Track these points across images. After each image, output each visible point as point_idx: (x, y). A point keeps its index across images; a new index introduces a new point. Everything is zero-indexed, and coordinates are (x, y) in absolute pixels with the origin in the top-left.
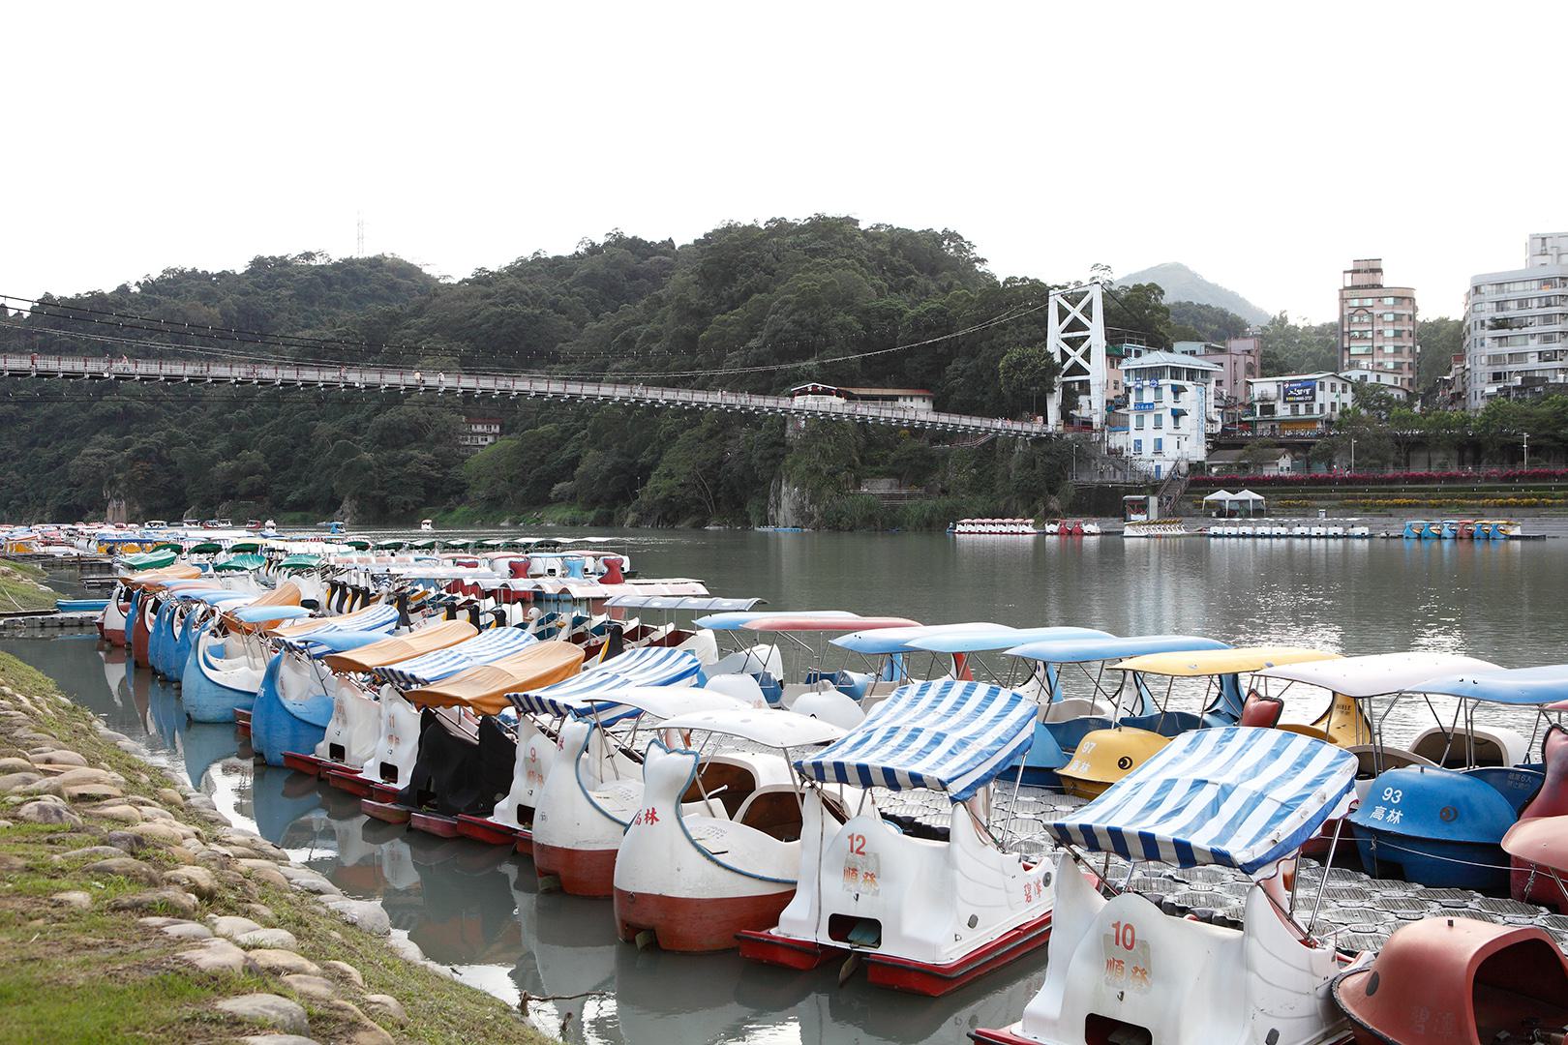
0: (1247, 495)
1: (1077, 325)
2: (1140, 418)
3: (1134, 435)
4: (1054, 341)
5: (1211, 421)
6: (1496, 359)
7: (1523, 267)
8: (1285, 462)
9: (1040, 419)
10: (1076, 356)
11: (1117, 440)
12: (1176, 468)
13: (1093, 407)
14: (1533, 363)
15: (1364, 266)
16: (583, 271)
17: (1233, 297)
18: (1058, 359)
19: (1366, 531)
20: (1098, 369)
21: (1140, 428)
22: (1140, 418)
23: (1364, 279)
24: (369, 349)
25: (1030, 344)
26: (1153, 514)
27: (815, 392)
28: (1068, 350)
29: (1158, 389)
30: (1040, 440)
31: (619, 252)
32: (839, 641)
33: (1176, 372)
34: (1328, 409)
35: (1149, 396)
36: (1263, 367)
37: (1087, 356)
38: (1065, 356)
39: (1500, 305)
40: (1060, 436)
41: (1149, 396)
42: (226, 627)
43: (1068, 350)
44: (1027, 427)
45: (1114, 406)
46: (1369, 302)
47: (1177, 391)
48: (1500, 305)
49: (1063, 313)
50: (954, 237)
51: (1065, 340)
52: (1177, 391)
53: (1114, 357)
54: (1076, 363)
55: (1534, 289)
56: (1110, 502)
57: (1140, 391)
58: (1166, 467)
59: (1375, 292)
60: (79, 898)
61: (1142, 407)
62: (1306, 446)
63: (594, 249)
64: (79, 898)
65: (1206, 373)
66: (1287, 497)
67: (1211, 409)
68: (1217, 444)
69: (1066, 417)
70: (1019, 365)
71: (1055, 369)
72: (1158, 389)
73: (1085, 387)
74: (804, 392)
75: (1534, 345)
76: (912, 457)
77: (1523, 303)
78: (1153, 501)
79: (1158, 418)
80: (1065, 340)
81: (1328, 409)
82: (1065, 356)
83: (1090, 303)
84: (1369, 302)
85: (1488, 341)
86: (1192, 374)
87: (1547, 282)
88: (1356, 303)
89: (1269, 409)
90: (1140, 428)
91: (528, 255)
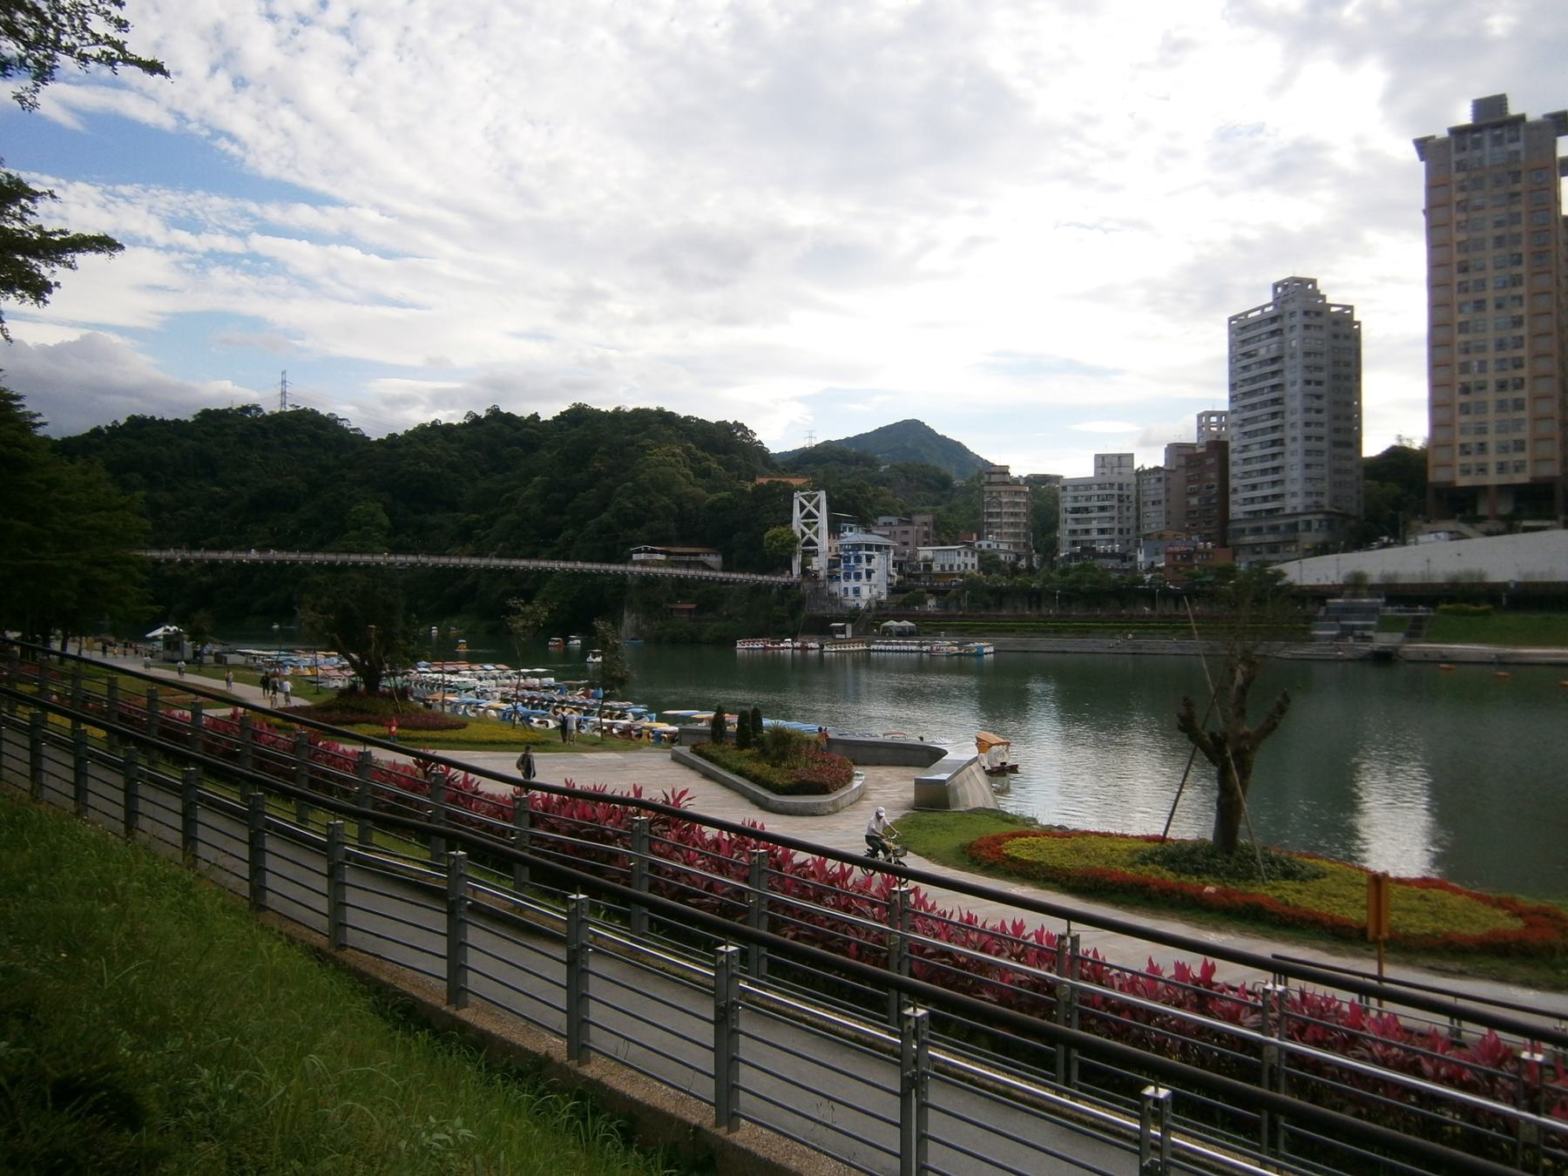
0: (905, 623)
1: (810, 515)
6: (1074, 532)
7: (1092, 474)
8: (931, 603)
11: (835, 588)
12: (869, 602)
13: (819, 564)
19: (1098, 562)
20: (824, 542)
24: (973, 1030)
25: (783, 525)
26: (849, 635)
27: (646, 551)
30: (787, 587)
31: (496, 425)
33: (869, 547)
37: (816, 533)
38: (803, 534)
39: (1076, 499)
40: (799, 585)
44: (779, 579)
45: (833, 564)
47: (869, 559)
48: (1076, 499)
49: (802, 507)
50: (741, 427)
53: (835, 529)
55: (1095, 491)
56: (822, 628)
58: (863, 605)
62: (945, 593)
63: (476, 421)
65: (887, 547)
66: (927, 627)
68: (893, 590)
70: (774, 538)
71: (796, 541)
74: (639, 552)
75: (1094, 525)
76: (709, 598)
77: (1088, 499)
78: (849, 626)
82: (803, 534)
86: (879, 548)
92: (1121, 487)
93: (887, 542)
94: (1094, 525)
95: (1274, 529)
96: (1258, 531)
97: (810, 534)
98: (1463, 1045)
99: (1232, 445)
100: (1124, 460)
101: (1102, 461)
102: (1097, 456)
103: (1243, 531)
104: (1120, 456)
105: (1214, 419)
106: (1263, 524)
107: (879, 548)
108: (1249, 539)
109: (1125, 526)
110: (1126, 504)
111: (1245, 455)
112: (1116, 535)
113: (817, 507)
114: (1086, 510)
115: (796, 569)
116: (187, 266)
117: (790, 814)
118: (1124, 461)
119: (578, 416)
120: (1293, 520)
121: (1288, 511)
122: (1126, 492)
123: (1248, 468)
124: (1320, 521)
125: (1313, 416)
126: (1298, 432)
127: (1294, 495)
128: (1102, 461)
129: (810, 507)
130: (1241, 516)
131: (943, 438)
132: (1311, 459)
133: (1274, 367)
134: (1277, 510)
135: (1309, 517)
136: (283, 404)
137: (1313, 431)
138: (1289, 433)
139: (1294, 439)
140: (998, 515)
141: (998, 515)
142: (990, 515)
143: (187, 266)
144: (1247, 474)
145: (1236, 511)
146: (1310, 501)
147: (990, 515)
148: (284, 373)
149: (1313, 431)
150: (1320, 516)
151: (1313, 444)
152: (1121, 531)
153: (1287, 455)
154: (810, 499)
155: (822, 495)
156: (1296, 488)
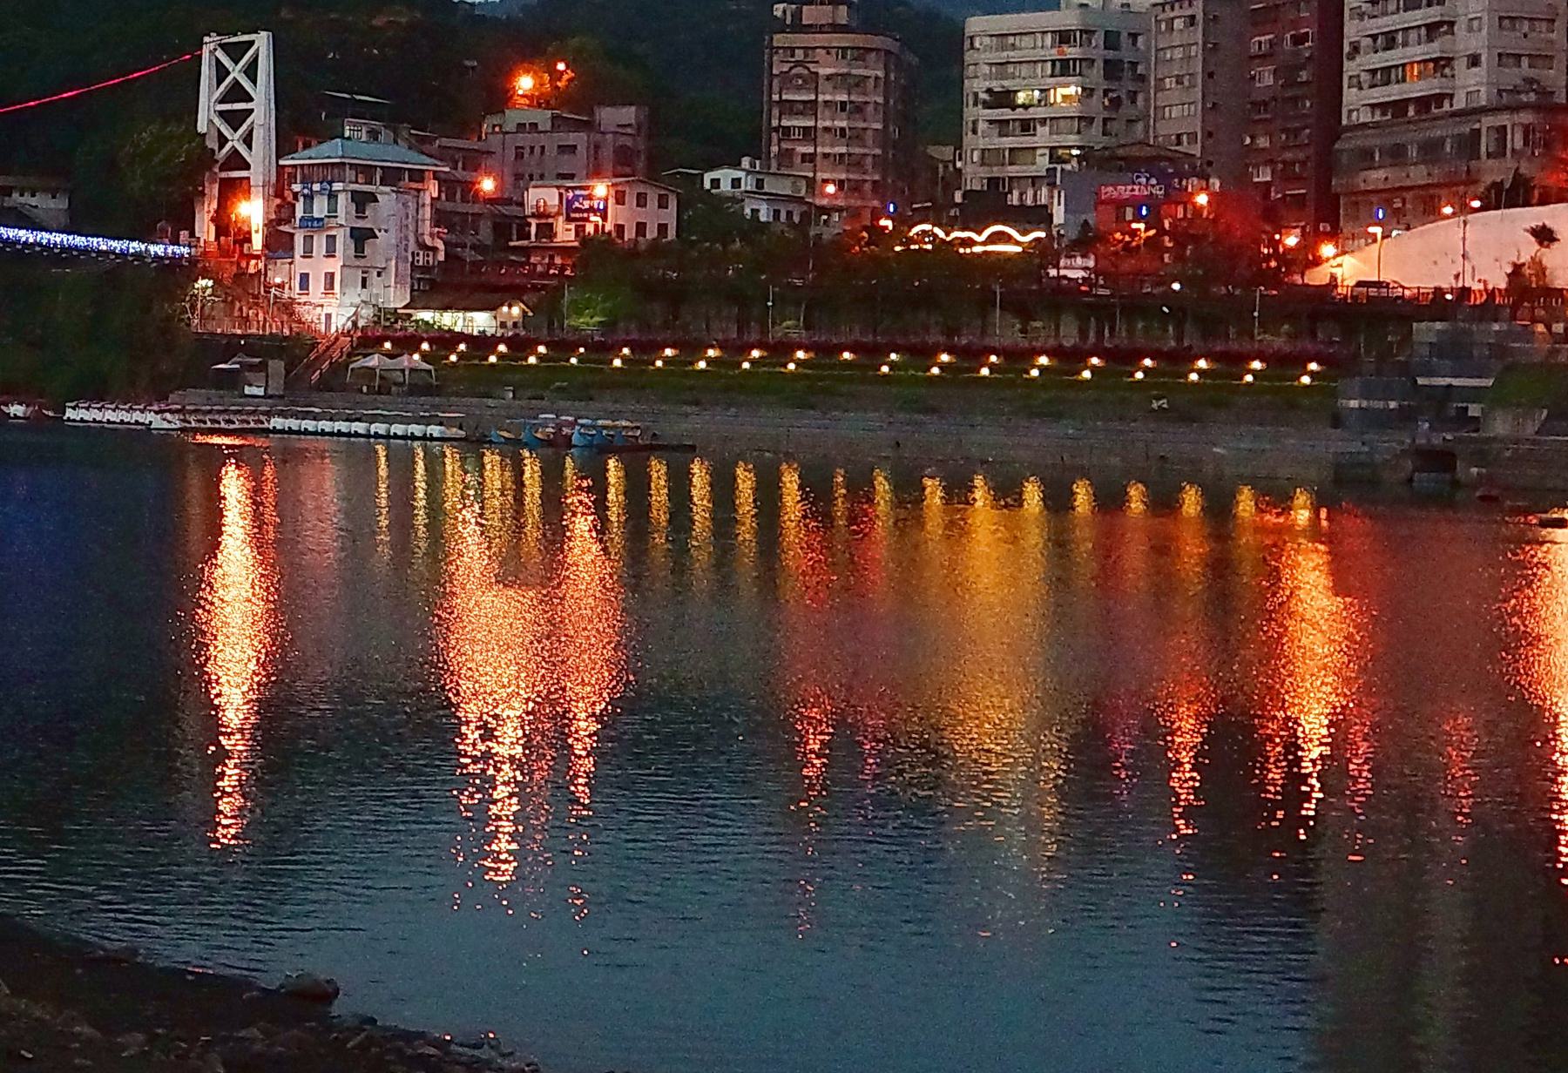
2: (308, 240)
3: (301, 265)
4: (207, 114)
5: (423, 246)
18: (212, 143)
21: (308, 254)
22: (308, 240)
29: (332, 196)
33: (367, 172)
35: (320, 208)
36: (651, 159)
37: (248, 140)
41: (320, 208)
49: (222, 72)
51: (221, 114)
52: (362, 201)
57: (309, 198)
60: (846, 355)
61: (311, 223)
64: (846, 355)
65: (417, 176)
67: (427, 227)
72: (332, 196)
79: (331, 239)
80: (221, 114)
82: (223, 140)
83: (255, 60)
85: (982, 126)
89: (547, 230)
90: (308, 254)
93: (417, 161)
96: (1396, 155)
97: (235, 140)
107: (391, 177)
108: (1376, 177)
113: (251, 72)
115: (205, 230)
116: (468, 761)
121: (1460, 103)
124: (1527, 130)
130: (1365, 117)
134: (1439, 99)
135: (1504, 119)
140: (810, 108)
141: (810, 108)
142: (789, 108)
143: (468, 761)
145: (1357, 102)
146: (1513, 76)
147: (789, 108)
150: (1526, 117)
155: (262, 42)
156: (1477, 42)
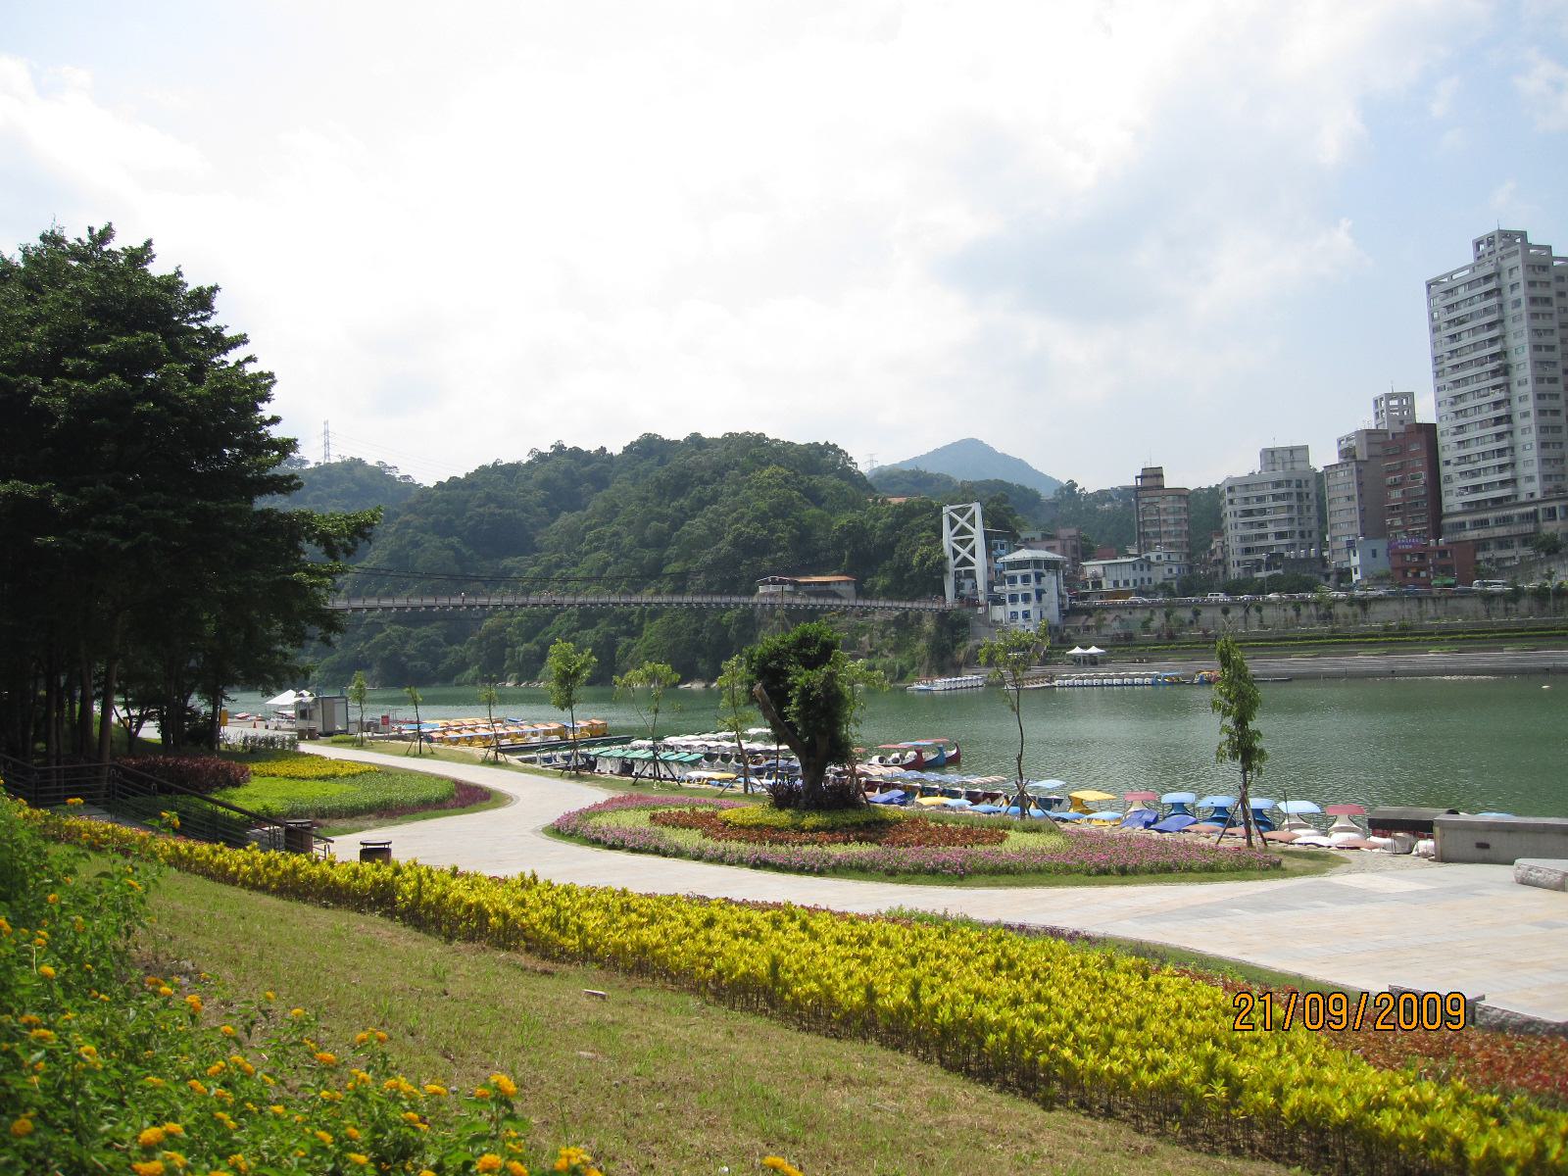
1: (963, 531)
6: (1244, 539)
9: (941, 597)
10: (964, 552)
14: (1272, 541)
15: (1150, 473)
16: (538, 476)
17: (1020, 465)
20: (980, 563)
23: (1149, 482)
27: (774, 582)
28: (958, 548)
32: (262, 503)
34: (1139, 583)
37: (972, 553)
42: (255, 774)
43: (958, 548)
46: (1156, 499)
47: (1039, 577)
49: (953, 523)
54: (965, 558)
59: (1160, 492)
63: (542, 457)
69: (959, 596)
73: (971, 574)
75: (1271, 529)
80: (955, 541)
81: (1139, 583)
82: (956, 553)
84: (1156, 499)
85: (1240, 526)
87: (1278, 484)
88: (1147, 500)
91: (489, 462)
92: (1299, 486)
94: (1271, 529)
95: (1506, 521)
96: (1482, 524)
98: (204, 1121)
99: (1440, 428)
100: (1298, 453)
101: (1270, 456)
102: (1306, 448)
103: (1462, 525)
104: (1292, 450)
105: (1394, 403)
106: (1490, 515)
109: (1306, 528)
110: (1306, 503)
111: (1460, 438)
112: (1297, 538)
114: (1263, 512)
117: (821, 873)
118: (1297, 455)
119: (649, 448)
120: (1531, 509)
121: (1523, 498)
122: (1305, 490)
123: (1464, 452)
125: (1546, 387)
126: (1529, 405)
127: (1530, 479)
128: (1270, 456)
129: (962, 521)
130: (1458, 508)
131: (1004, 456)
132: (1549, 437)
133: (1494, 333)
134: (1507, 498)
136: (327, 455)
137: (1548, 403)
138: (1519, 407)
139: (1526, 415)
144: (1464, 459)
145: (1452, 502)
146: (1550, 485)
148: (326, 423)
149: (1548, 403)
151: (1549, 420)
152: (1302, 534)
153: (1518, 433)
154: (962, 513)
155: (976, 508)
